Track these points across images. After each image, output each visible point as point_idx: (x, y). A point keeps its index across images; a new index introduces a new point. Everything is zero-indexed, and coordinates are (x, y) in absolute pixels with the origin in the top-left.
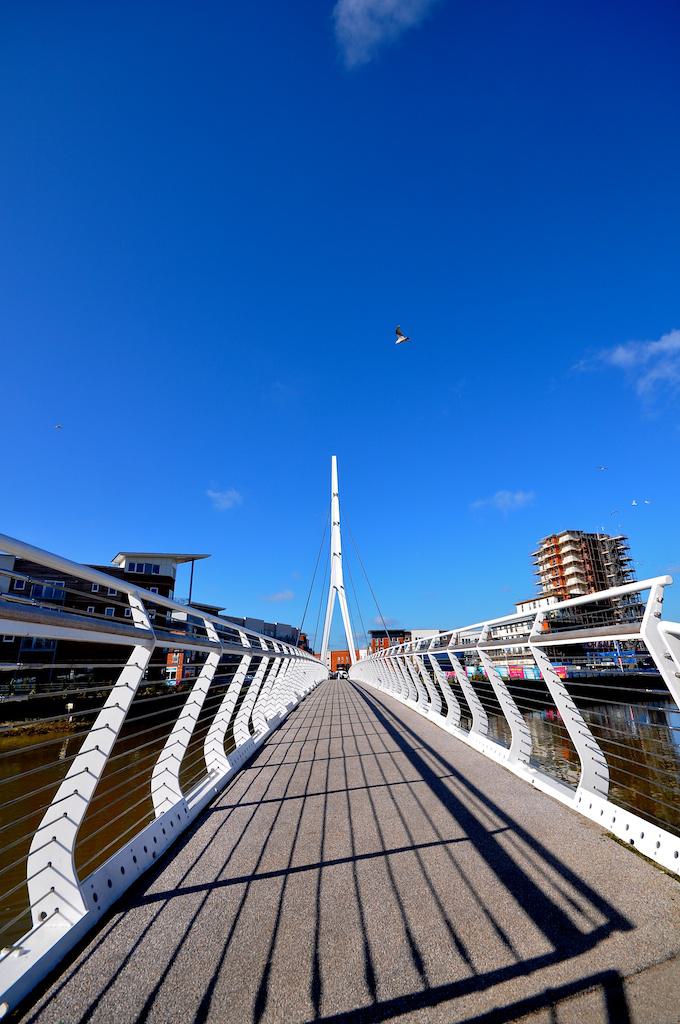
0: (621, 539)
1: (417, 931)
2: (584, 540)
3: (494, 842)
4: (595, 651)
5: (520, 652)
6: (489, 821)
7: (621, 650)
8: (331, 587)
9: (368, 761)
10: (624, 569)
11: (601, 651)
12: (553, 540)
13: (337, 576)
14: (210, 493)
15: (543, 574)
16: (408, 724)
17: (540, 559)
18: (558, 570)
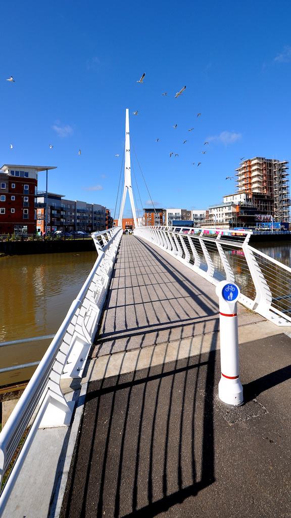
0: (285, 163)
1: (178, 312)
2: (265, 163)
3: (198, 297)
4: (261, 222)
5: (223, 222)
6: (196, 292)
7: (274, 222)
8: (125, 186)
9: (151, 276)
10: (284, 180)
11: (264, 222)
12: (248, 162)
13: (128, 181)
14: (56, 128)
15: (240, 181)
16: (169, 261)
17: (240, 173)
18: (249, 179)
